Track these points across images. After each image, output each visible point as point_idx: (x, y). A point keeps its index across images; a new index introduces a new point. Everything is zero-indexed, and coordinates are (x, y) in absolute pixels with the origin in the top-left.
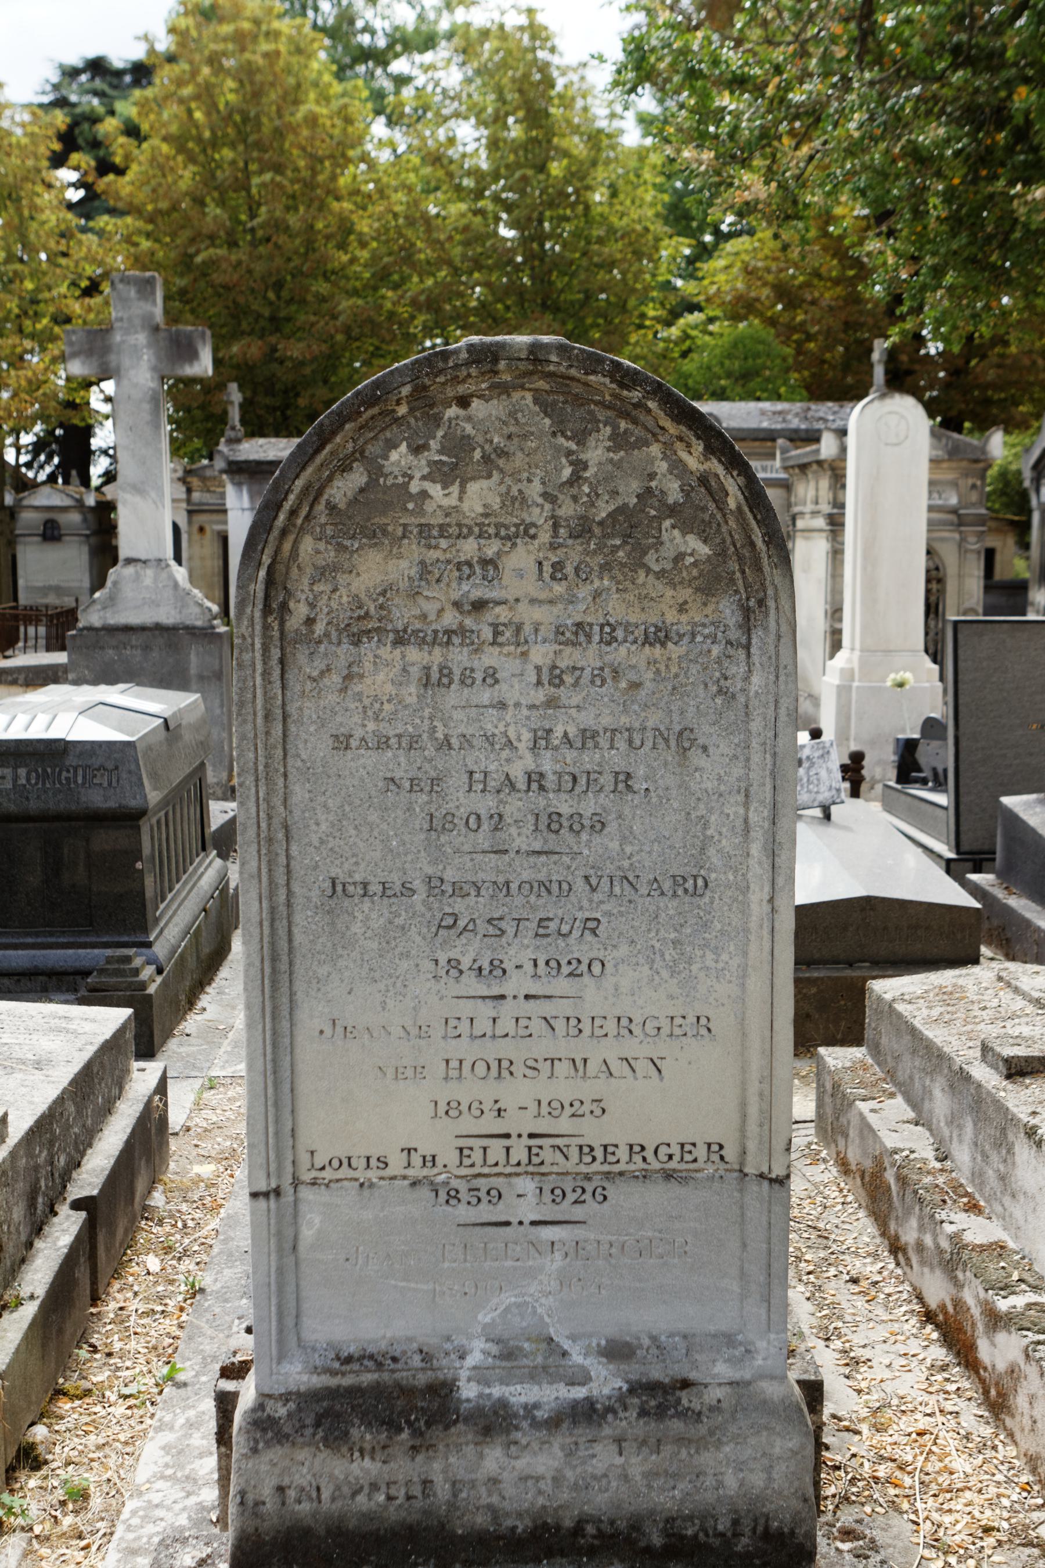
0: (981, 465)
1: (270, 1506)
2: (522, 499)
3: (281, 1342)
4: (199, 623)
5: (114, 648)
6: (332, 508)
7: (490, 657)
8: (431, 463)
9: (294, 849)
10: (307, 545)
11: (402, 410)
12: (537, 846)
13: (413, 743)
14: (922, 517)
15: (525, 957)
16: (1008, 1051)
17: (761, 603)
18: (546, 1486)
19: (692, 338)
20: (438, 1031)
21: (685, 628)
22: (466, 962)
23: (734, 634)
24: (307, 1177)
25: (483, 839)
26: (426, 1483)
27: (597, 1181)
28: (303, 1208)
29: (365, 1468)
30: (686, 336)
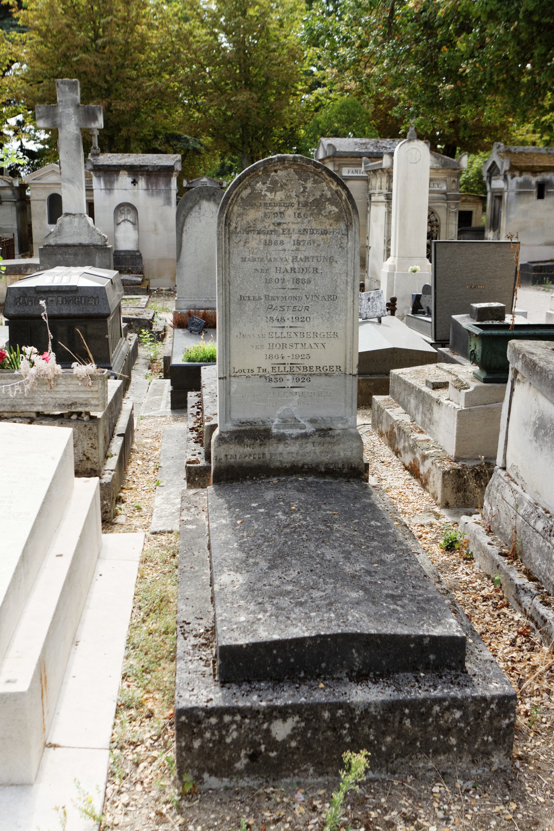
0: (458, 171)
1: (223, 460)
2: (290, 197)
3: (226, 418)
4: (99, 243)
5: (62, 254)
6: (242, 198)
7: (282, 238)
8: (267, 187)
9: (231, 288)
10: (236, 208)
11: (260, 173)
12: (293, 287)
13: (262, 260)
14: (427, 195)
15: (290, 316)
16: (433, 381)
17: (351, 224)
18: (294, 455)
19: (321, 101)
20: (267, 336)
21: (331, 230)
22: (275, 318)
23: (344, 232)
24: (233, 375)
25: (279, 285)
26: (264, 454)
27: (308, 376)
28: (232, 383)
29: (248, 450)
30: (317, 99)
